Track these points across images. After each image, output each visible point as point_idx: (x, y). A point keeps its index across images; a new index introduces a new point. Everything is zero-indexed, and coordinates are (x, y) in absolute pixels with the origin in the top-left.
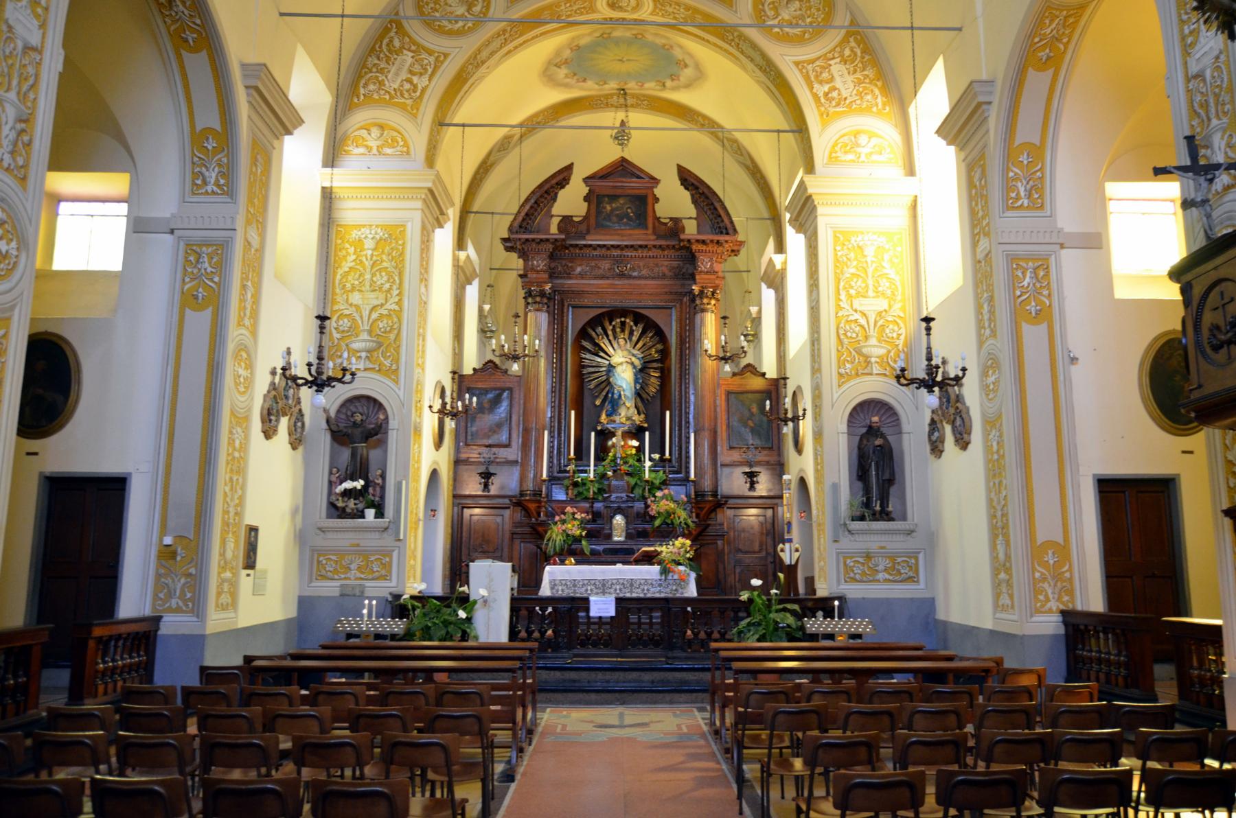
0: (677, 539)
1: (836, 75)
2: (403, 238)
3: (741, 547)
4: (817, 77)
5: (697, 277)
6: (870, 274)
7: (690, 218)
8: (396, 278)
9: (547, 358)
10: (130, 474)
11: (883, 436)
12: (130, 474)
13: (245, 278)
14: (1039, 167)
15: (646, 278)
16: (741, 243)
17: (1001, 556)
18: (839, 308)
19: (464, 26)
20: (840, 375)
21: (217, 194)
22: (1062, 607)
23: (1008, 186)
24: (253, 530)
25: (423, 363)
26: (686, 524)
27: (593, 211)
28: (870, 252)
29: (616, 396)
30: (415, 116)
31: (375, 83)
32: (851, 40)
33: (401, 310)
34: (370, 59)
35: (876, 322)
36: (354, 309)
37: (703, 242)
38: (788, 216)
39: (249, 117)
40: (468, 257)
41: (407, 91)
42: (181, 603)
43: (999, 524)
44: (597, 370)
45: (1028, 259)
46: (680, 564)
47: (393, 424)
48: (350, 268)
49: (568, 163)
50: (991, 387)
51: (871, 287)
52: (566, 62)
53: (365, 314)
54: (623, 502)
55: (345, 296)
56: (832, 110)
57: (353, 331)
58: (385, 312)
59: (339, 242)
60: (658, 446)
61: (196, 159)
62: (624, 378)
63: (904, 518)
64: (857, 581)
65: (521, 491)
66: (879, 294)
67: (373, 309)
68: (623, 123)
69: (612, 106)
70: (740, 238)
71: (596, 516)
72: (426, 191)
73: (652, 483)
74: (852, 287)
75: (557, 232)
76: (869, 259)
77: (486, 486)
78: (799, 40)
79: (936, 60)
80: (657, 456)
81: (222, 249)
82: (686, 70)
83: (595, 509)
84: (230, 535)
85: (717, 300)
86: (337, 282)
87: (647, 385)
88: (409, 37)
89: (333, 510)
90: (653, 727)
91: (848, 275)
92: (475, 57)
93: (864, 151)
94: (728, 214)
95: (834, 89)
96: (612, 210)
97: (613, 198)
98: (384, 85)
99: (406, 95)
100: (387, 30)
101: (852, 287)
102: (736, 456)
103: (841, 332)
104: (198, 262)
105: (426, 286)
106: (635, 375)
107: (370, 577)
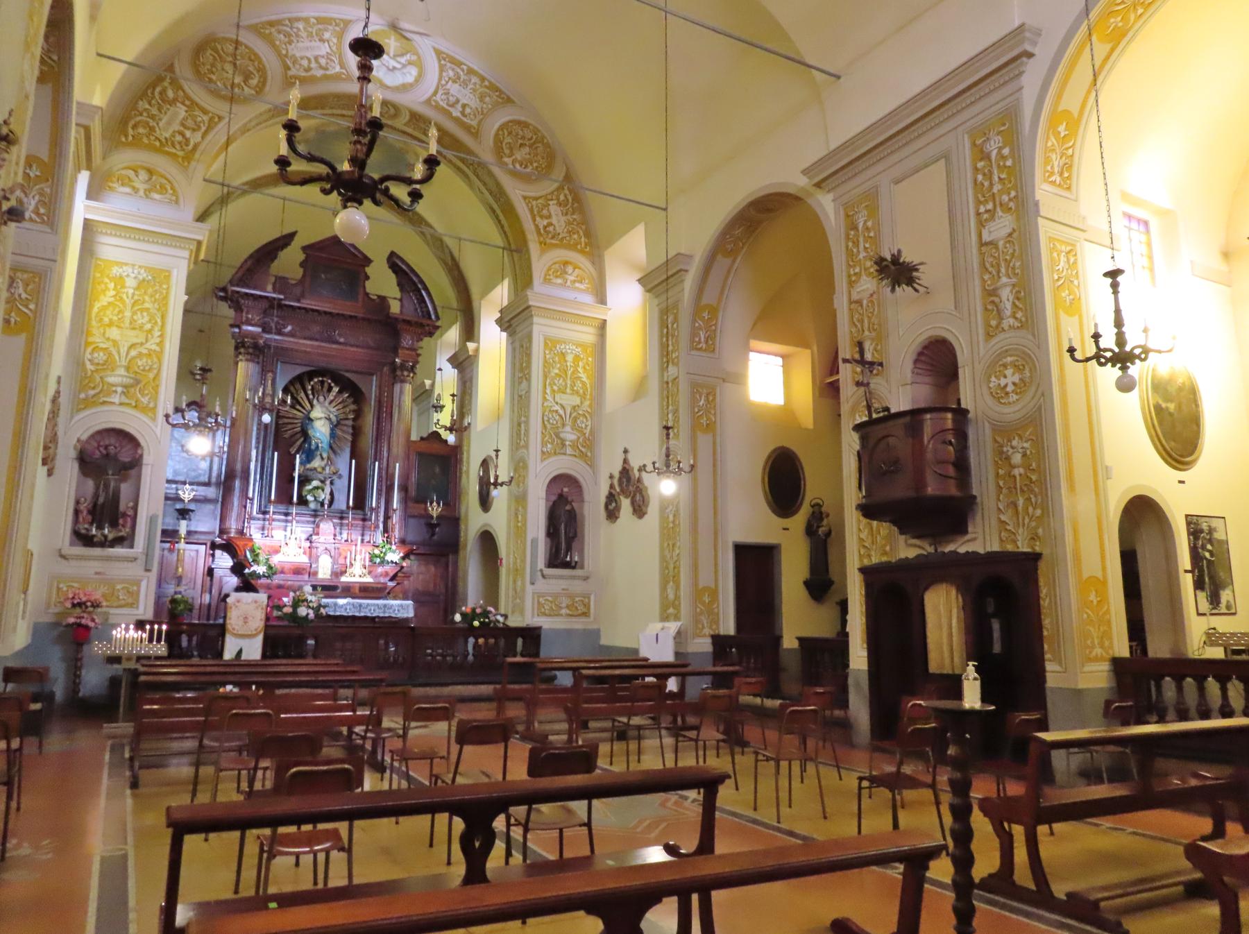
2: (168, 284)
4: (539, 212)
7: (395, 299)
14: (1071, 144)
17: (671, 596)
18: (545, 398)
20: (543, 453)
21: (36, 222)
22: (712, 633)
23: (694, 333)
28: (570, 358)
29: (313, 447)
31: (145, 128)
33: (162, 351)
34: (141, 103)
35: (571, 414)
36: (111, 343)
41: (180, 143)
43: (671, 574)
47: (147, 459)
48: (109, 303)
53: (123, 350)
57: (108, 365)
58: (145, 351)
59: (98, 275)
63: (582, 567)
64: (546, 615)
67: (133, 346)
86: (93, 315)
88: (184, 91)
100: (160, 79)
103: (546, 418)
107: (115, 604)
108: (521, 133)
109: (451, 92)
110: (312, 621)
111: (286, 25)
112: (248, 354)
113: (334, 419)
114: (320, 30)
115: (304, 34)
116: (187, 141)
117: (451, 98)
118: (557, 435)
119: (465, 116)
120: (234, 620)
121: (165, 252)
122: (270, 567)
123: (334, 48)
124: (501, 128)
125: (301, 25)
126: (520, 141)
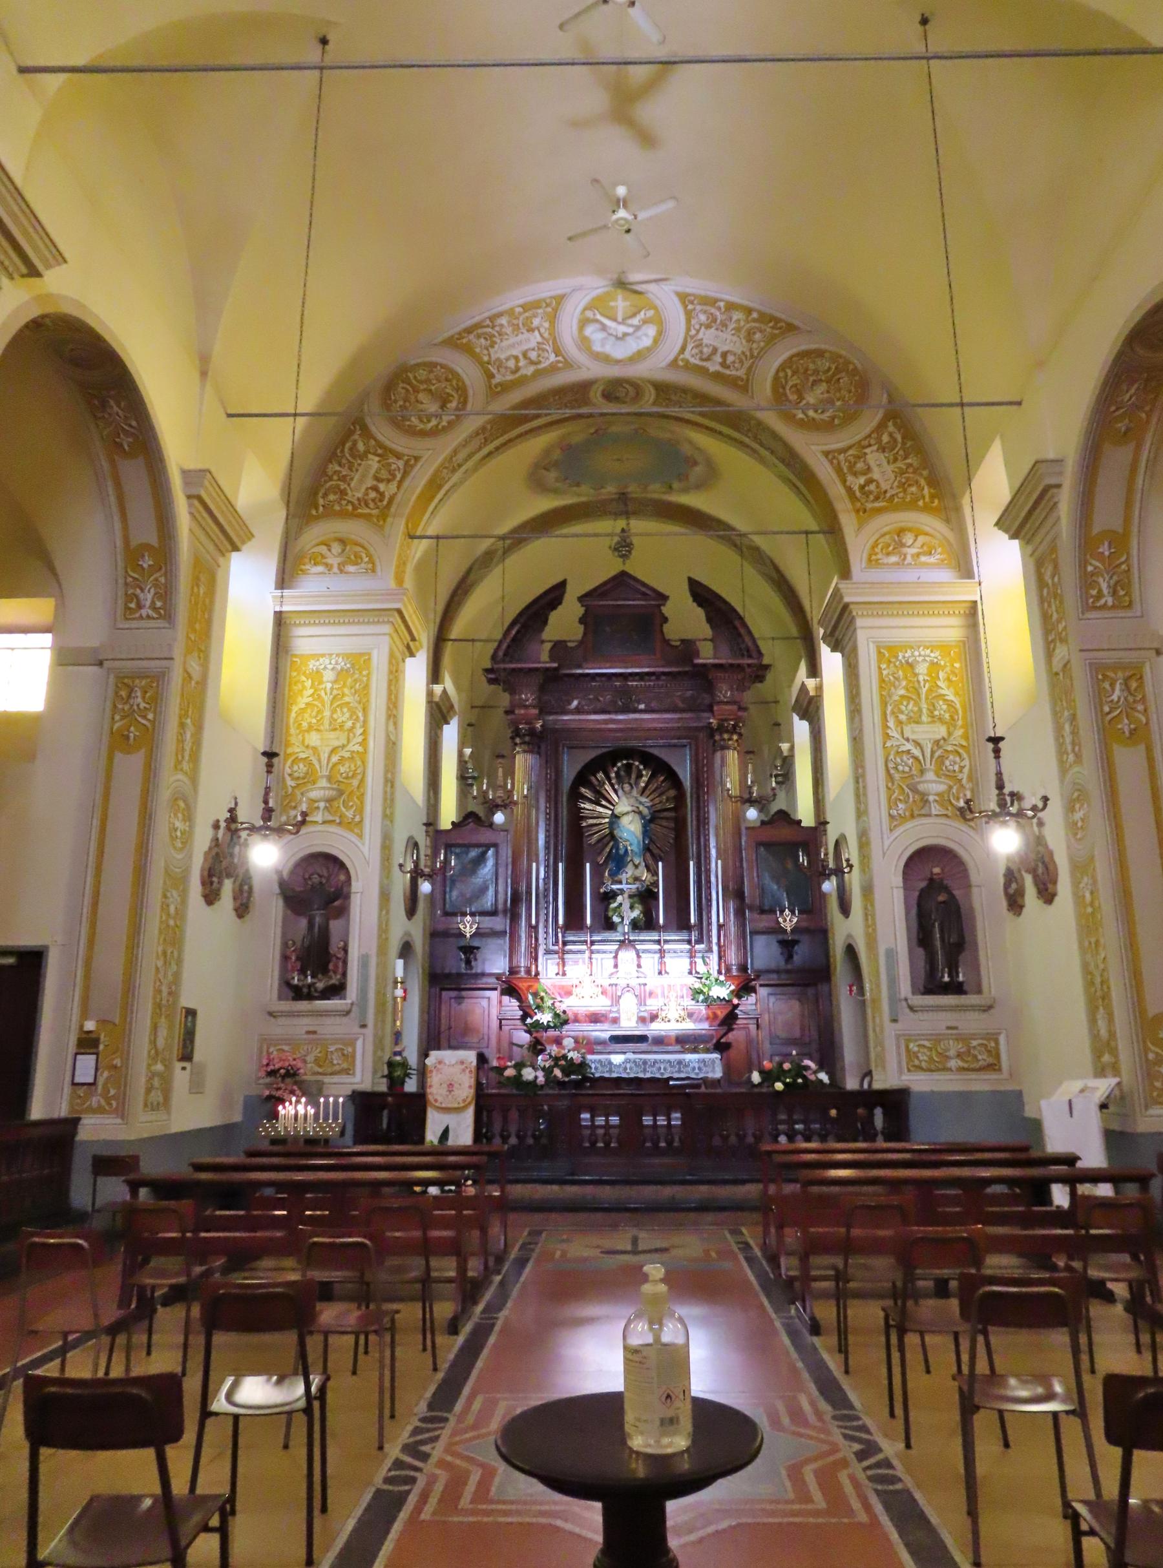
1: (872, 463)
2: (368, 668)
5: (715, 708)
6: (923, 696)
7: (705, 640)
10: (46, 948)
11: (947, 890)
12: (46, 948)
13: (183, 716)
16: (767, 667)
17: (1104, 1032)
18: (887, 737)
19: (437, 426)
23: (1087, 581)
24: (191, 1013)
25: (392, 814)
28: (922, 669)
29: (622, 852)
30: (382, 528)
31: (335, 493)
32: (890, 424)
34: (330, 466)
35: (933, 753)
36: (311, 751)
38: (822, 631)
39: (190, 530)
40: (445, 691)
41: (373, 500)
42: (103, 1102)
45: (1116, 667)
48: (307, 704)
49: (559, 579)
50: (1080, 824)
51: (924, 711)
52: (556, 464)
55: (300, 737)
57: (308, 779)
58: (347, 755)
59: (294, 674)
61: (129, 580)
62: (631, 830)
63: (979, 991)
64: (921, 1069)
66: (935, 719)
68: (623, 530)
69: (610, 513)
70: (766, 661)
74: (902, 712)
75: (547, 659)
76: (921, 678)
78: (828, 427)
79: (992, 441)
81: (156, 681)
84: (163, 1019)
85: (740, 735)
86: (292, 721)
88: (376, 440)
89: (286, 990)
90: (674, 1252)
91: (897, 698)
99: (372, 505)
100: (350, 433)
101: (902, 712)
103: (891, 765)
104: (129, 697)
105: (395, 724)
107: (329, 1070)
108: (812, 366)
109: (705, 342)
110: (542, 1086)
111: (488, 326)
112: (524, 743)
113: (646, 811)
114: (527, 318)
115: (509, 330)
116: (382, 494)
117: (705, 350)
118: (915, 790)
119: (728, 367)
120: (436, 1090)
121: (368, 631)
122: (556, 1015)
123: (546, 335)
124: (782, 368)
125: (504, 321)
126: (811, 379)
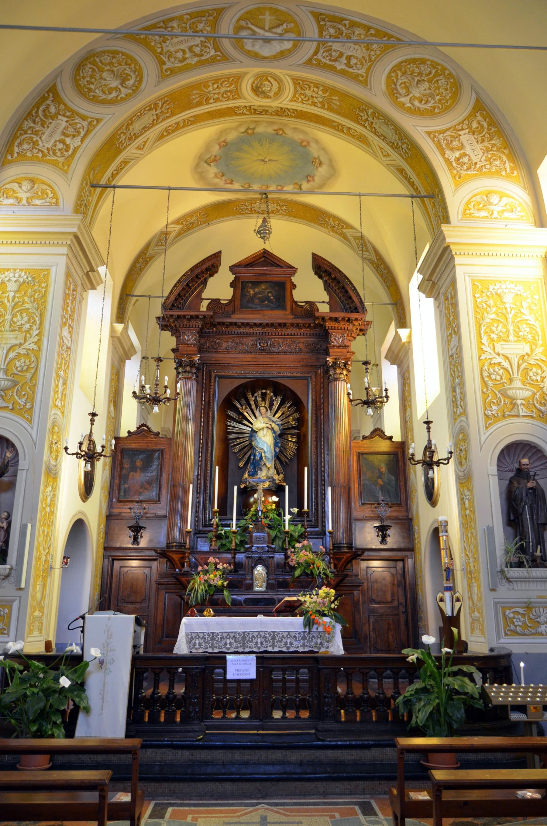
0: (320, 588)
1: (465, 143)
2: (47, 282)
3: (374, 597)
4: (448, 144)
5: (331, 350)
6: (510, 320)
7: (323, 302)
8: (37, 319)
9: (195, 421)
15: (285, 353)
16: (369, 323)
18: (482, 351)
19: (117, 96)
26: (325, 574)
27: (238, 295)
28: (508, 299)
29: (257, 458)
31: (29, 143)
32: (478, 114)
34: (26, 123)
35: (519, 366)
37: (336, 320)
44: (240, 436)
46: (324, 615)
47: (23, 463)
51: (511, 332)
52: (215, 160)
54: (265, 553)
56: (463, 173)
58: (23, 352)
60: (298, 501)
65: (167, 543)
66: (519, 338)
70: (368, 317)
71: (238, 566)
72: (71, 237)
73: (291, 535)
74: (493, 332)
76: (508, 306)
77: (136, 540)
78: (430, 114)
80: (295, 510)
82: (320, 169)
83: (237, 560)
85: (349, 371)
87: (285, 449)
88: (65, 105)
91: (489, 321)
92: (127, 128)
93: (496, 209)
94: (358, 295)
95: (465, 155)
96: (255, 294)
97: (256, 284)
98: (38, 145)
99: (59, 154)
100: (44, 99)
101: (493, 332)
102: (367, 511)
103: (485, 374)
106: (275, 439)
